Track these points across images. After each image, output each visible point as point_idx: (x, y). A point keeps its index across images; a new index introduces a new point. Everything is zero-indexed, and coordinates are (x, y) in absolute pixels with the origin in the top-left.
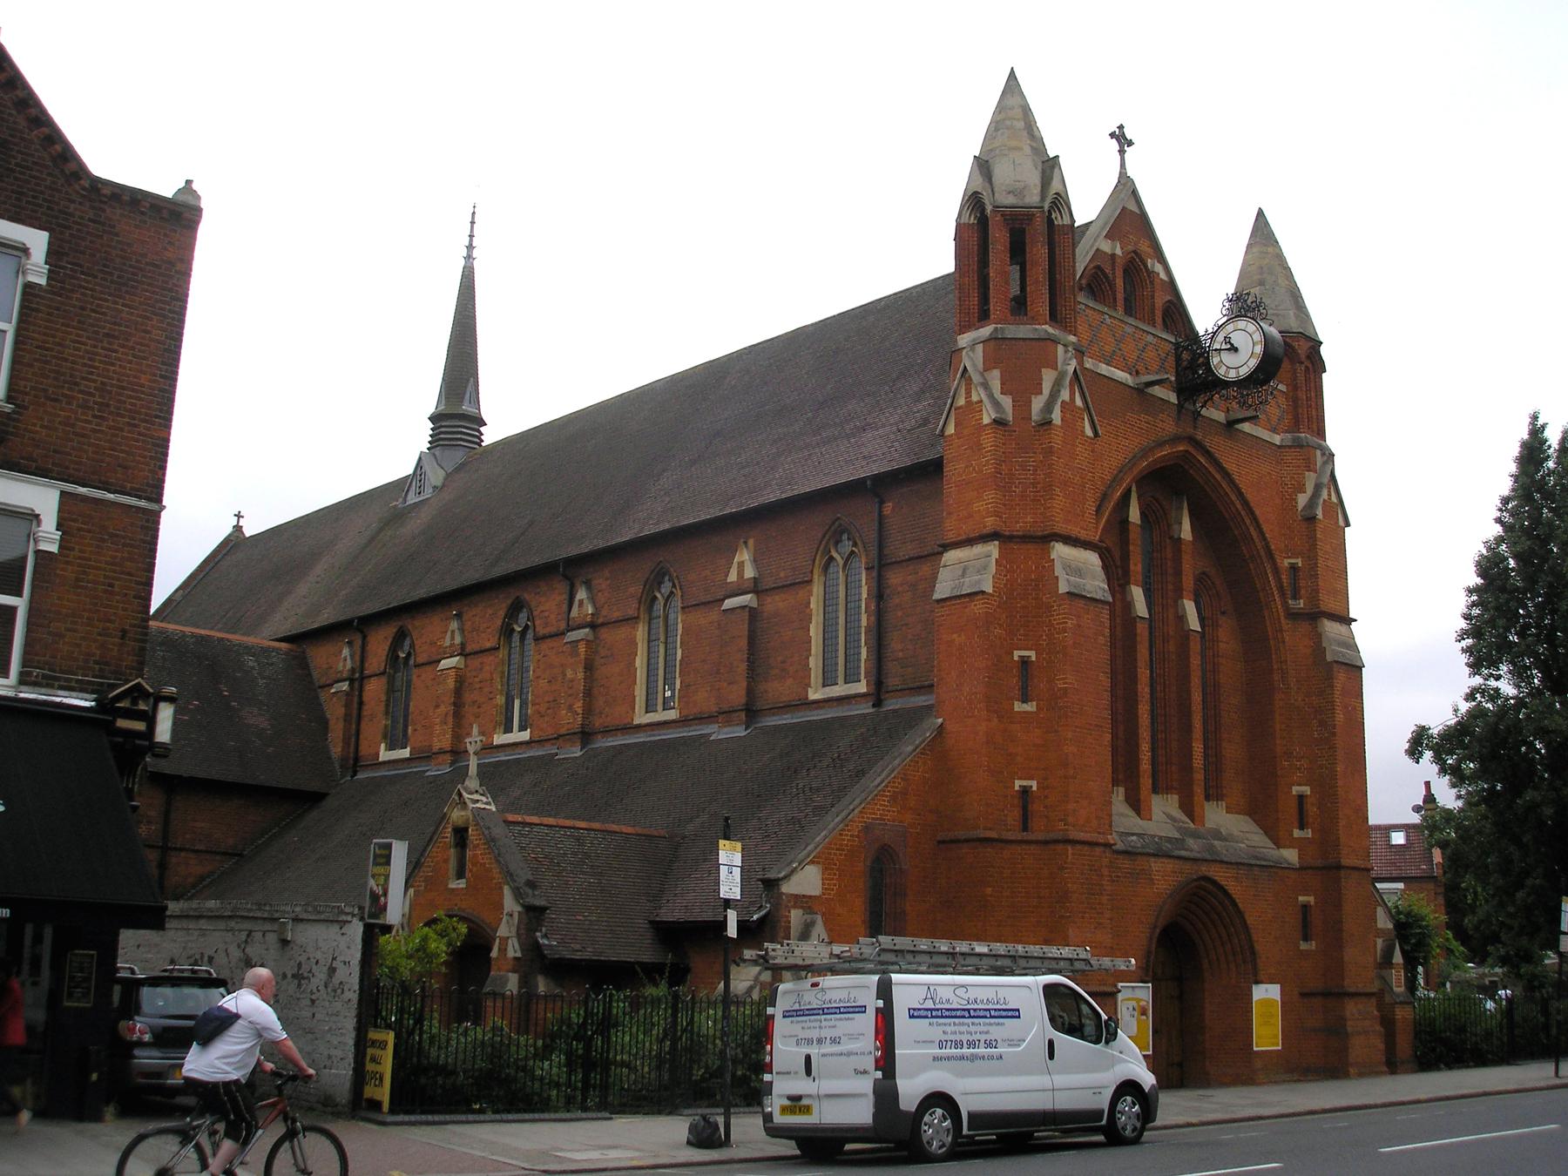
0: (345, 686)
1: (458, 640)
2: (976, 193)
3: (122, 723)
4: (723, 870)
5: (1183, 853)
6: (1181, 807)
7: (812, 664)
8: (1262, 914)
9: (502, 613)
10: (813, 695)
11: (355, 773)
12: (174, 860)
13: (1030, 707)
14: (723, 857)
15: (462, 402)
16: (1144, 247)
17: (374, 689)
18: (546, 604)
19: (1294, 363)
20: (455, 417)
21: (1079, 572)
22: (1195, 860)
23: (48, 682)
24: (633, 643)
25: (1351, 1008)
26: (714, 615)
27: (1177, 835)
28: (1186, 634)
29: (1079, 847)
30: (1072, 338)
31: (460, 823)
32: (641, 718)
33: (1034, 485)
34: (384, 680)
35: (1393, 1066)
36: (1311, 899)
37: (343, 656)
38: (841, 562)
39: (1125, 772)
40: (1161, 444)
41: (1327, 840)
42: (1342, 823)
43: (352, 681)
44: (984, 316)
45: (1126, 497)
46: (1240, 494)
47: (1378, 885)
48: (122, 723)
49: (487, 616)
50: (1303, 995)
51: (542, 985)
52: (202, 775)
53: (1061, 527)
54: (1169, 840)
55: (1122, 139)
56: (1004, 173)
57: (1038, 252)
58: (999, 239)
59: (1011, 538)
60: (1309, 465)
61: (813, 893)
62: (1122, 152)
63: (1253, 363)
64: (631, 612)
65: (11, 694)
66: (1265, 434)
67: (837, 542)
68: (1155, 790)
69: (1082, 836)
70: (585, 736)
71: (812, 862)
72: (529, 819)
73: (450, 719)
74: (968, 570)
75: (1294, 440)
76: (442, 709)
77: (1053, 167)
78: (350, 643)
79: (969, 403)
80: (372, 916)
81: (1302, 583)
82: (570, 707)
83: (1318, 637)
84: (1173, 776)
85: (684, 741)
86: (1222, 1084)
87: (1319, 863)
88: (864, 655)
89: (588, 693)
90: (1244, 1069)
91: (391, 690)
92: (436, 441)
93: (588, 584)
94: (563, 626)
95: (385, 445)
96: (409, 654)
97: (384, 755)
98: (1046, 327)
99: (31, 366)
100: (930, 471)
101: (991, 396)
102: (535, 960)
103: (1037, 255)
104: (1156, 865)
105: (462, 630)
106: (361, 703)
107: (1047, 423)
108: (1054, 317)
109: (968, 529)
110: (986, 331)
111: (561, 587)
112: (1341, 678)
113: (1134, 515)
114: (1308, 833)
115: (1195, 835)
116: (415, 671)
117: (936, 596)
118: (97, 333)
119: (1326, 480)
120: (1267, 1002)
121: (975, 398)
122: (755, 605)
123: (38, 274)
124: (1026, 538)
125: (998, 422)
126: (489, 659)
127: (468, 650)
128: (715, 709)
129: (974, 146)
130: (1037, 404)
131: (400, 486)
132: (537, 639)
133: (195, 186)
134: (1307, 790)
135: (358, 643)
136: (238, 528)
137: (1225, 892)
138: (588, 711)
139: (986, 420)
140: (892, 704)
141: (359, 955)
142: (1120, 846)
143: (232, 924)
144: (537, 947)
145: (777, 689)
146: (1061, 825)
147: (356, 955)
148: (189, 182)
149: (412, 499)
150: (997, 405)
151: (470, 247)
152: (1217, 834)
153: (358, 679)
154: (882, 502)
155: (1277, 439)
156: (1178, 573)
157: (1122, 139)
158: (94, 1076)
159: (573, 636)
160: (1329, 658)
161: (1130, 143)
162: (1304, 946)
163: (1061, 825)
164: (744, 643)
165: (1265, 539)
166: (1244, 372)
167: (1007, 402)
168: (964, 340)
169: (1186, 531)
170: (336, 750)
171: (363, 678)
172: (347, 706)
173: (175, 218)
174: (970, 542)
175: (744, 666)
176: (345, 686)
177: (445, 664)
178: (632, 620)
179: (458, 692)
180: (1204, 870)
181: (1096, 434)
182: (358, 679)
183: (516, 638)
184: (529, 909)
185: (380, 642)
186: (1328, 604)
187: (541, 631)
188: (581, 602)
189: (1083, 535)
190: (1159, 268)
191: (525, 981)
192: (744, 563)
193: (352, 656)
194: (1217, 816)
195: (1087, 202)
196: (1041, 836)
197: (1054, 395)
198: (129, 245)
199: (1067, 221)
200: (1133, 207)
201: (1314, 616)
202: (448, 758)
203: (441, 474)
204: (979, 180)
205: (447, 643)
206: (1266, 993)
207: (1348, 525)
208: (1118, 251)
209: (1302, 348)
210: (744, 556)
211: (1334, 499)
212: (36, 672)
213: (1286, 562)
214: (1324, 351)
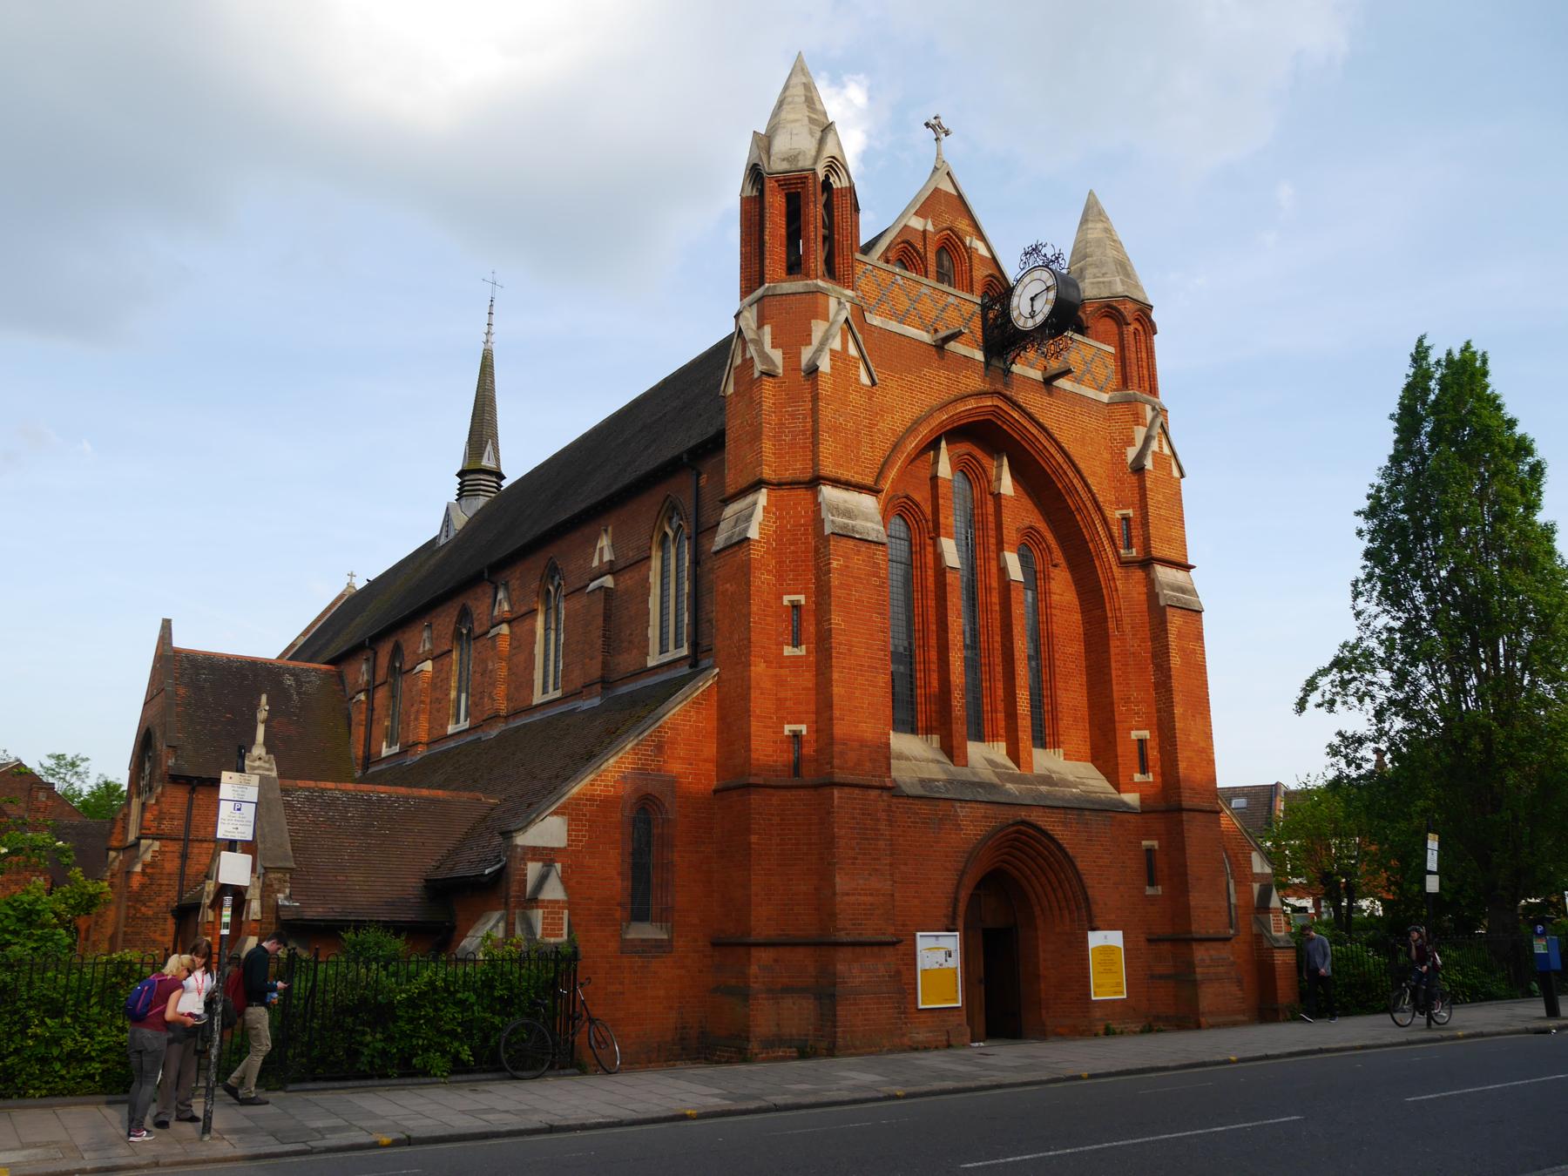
0: (362, 697)
2: (755, 165)
6: (1009, 753)
7: (650, 634)
8: (1100, 864)
12: (196, 851)
16: (962, 225)
20: (474, 475)
21: (848, 513)
24: (533, 633)
25: (1201, 953)
27: (995, 780)
29: (847, 790)
30: (849, 292)
35: (1266, 1011)
36: (1155, 844)
57: (815, 211)
58: (776, 203)
60: (1138, 419)
61: (556, 845)
66: (1090, 393)
69: (851, 778)
71: (555, 813)
78: (367, 660)
79: (744, 360)
83: (1151, 582)
86: (1061, 1035)
90: (1084, 1020)
104: (962, 811)
107: (813, 371)
108: (831, 272)
112: (1175, 621)
114: (1151, 778)
120: (1107, 950)
124: (793, 484)
134: (1146, 734)
150: (766, 358)
154: (699, 474)
155: (1105, 398)
160: (1162, 603)
162: (1149, 891)
165: (1090, 490)
169: (1007, 486)
176: (362, 697)
181: (874, 383)
182: (370, 690)
185: (385, 650)
186: (1159, 550)
189: (857, 479)
192: (605, 549)
194: (1046, 761)
197: (823, 343)
200: (947, 187)
201: (1147, 563)
206: (1105, 941)
207: (1182, 476)
208: (930, 228)
209: (1128, 310)
210: (604, 542)
211: (1166, 451)
213: (1118, 514)
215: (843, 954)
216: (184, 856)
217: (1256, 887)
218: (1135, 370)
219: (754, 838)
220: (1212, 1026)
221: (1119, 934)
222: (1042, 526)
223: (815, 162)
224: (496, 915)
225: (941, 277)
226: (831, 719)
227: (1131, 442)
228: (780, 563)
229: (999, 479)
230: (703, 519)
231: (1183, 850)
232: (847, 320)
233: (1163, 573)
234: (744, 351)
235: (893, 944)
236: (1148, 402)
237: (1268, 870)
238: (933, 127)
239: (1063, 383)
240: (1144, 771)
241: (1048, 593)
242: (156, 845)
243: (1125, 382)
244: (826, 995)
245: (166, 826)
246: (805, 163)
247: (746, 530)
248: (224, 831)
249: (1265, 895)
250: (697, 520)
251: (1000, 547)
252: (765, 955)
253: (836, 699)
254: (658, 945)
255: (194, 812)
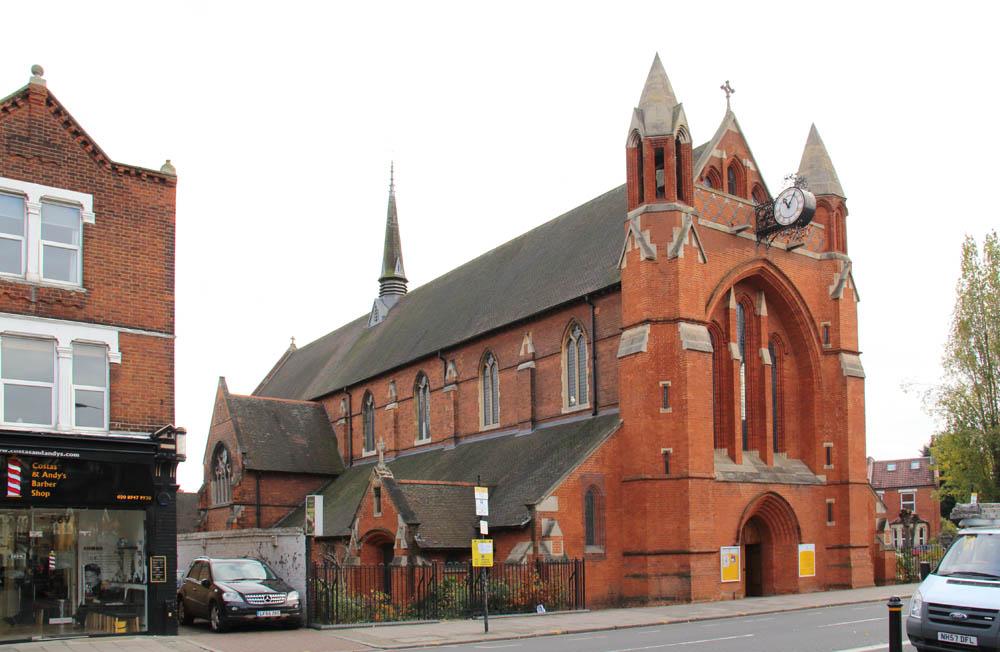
0: (343, 421)
1: (394, 394)
3: (163, 446)
4: (478, 502)
5: (760, 481)
6: (761, 457)
7: (563, 395)
8: (803, 508)
9: (413, 380)
10: (564, 411)
11: (352, 464)
13: (669, 410)
14: (477, 495)
15: (394, 270)
17: (357, 422)
18: (434, 372)
19: (827, 213)
20: (391, 281)
21: (694, 337)
22: (765, 483)
23: (125, 428)
24: (476, 390)
25: (853, 554)
26: (514, 373)
27: (756, 471)
28: (763, 367)
30: (691, 209)
31: (377, 486)
32: (483, 428)
33: (669, 292)
34: (361, 417)
37: (337, 408)
38: (575, 341)
39: (723, 437)
40: (747, 263)
41: (842, 469)
42: (850, 460)
43: (346, 418)
44: (641, 200)
45: (728, 292)
46: (795, 289)
47: (878, 492)
48: (163, 446)
49: (407, 380)
50: (828, 549)
51: (419, 561)
52: (273, 469)
53: (684, 314)
54: (752, 474)
55: (727, 89)
56: (651, 117)
59: (657, 322)
60: (836, 269)
62: (728, 97)
63: (798, 214)
64: (475, 375)
65: (104, 435)
66: (810, 254)
67: (573, 331)
68: (746, 448)
70: (456, 438)
71: (553, 495)
72: (412, 481)
73: (393, 434)
74: (637, 340)
75: (828, 256)
76: (389, 430)
77: (679, 109)
80: (309, 532)
81: (831, 335)
82: (448, 425)
83: (839, 363)
84: (753, 440)
85: (503, 439)
87: (838, 481)
88: (588, 390)
89: (456, 417)
90: (792, 587)
91: (365, 422)
92: (383, 292)
93: (453, 361)
94: (443, 384)
95: (349, 297)
96: (372, 404)
97: (365, 454)
98: (676, 204)
99: (93, 267)
100: (615, 289)
101: (645, 245)
102: (414, 549)
103: (659, 159)
104: (743, 487)
105: (395, 390)
106: (352, 429)
108: (680, 197)
109: (635, 319)
110: (642, 208)
111: (441, 364)
112: (851, 384)
113: (733, 304)
115: (767, 471)
116: (375, 412)
117: (619, 356)
118: (127, 248)
119: (846, 276)
120: (807, 554)
121: (636, 247)
122: (534, 366)
123: (90, 218)
124: (666, 321)
125: (650, 259)
126: (409, 403)
127: (399, 399)
128: (517, 422)
129: (635, 102)
130: (670, 247)
131: (367, 318)
132: (431, 392)
133: (172, 163)
134: (831, 444)
135: (348, 400)
136: (293, 345)
137: (784, 500)
138: (457, 426)
139: (642, 258)
140: (602, 413)
141: (305, 551)
142: (721, 477)
143: (254, 539)
144: (415, 542)
145: (545, 410)
146: (685, 470)
147: (303, 551)
148: (168, 161)
149: (373, 323)
150: (648, 250)
151: (392, 185)
152: (780, 470)
153: (349, 417)
154: (594, 308)
155: (818, 256)
156: (759, 334)
157: (727, 89)
158: (170, 614)
159: (447, 389)
160: (845, 374)
161: (733, 91)
162: (829, 524)
163: (685, 470)
164: (529, 387)
165: (809, 312)
166: (793, 219)
167: (653, 248)
168: (631, 214)
169: (764, 311)
170: (342, 453)
171: (351, 417)
172: (345, 431)
173: (164, 181)
174: (635, 325)
175: (529, 398)
176: (343, 421)
177: (388, 407)
178: (475, 379)
179: (396, 421)
180: (771, 488)
181: (705, 262)
182: (349, 417)
183: (421, 392)
184: (409, 525)
185: (358, 396)
187: (433, 387)
188: (450, 372)
189: (697, 317)
190: (749, 164)
191: (411, 560)
192: (527, 345)
193: (346, 406)
194: (779, 461)
195: (702, 131)
196: (674, 476)
198: (138, 198)
199: (688, 141)
201: (837, 352)
202: (394, 454)
203: (386, 310)
204: (637, 122)
205: (389, 396)
208: (725, 156)
209: (834, 203)
210: (527, 341)
211: (851, 287)
212: (117, 424)
213: (822, 324)
214: (848, 204)
215: (694, 557)
216: (258, 514)
217: (877, 521)
218: (836, 240)
219: (648, 505)
220: (857, 588)
221: (813, 545)
222: (779, 332)
223: (673, 130)
224: (528, 544)
225: (732, 191)
226: (687, 445)
227: (832, 283)
228: (658, 364)
229: (760, 307)
230: (597, 334)
231: (848, 503)
232: (692, 227)
233: (846, 358)
234: (633, 244)
235: (89, 548)
236: (843, 259)
237: (884, 512)
238: (725, 89)
239: (798, 251)
240: (829, 464)
241: (782, 369)
242: (243, 508)
243: (829, 248)
244: (685, 575)
245: (246, 498)
246: (667, 130)
247: (640, 346)
248: (479, 512)
249: (882, 525)
250: (594, 334)
251: (759, 344)
252: (652, 559)
253: (689, 435)
254: (600, 556)
255: (261, 489)
